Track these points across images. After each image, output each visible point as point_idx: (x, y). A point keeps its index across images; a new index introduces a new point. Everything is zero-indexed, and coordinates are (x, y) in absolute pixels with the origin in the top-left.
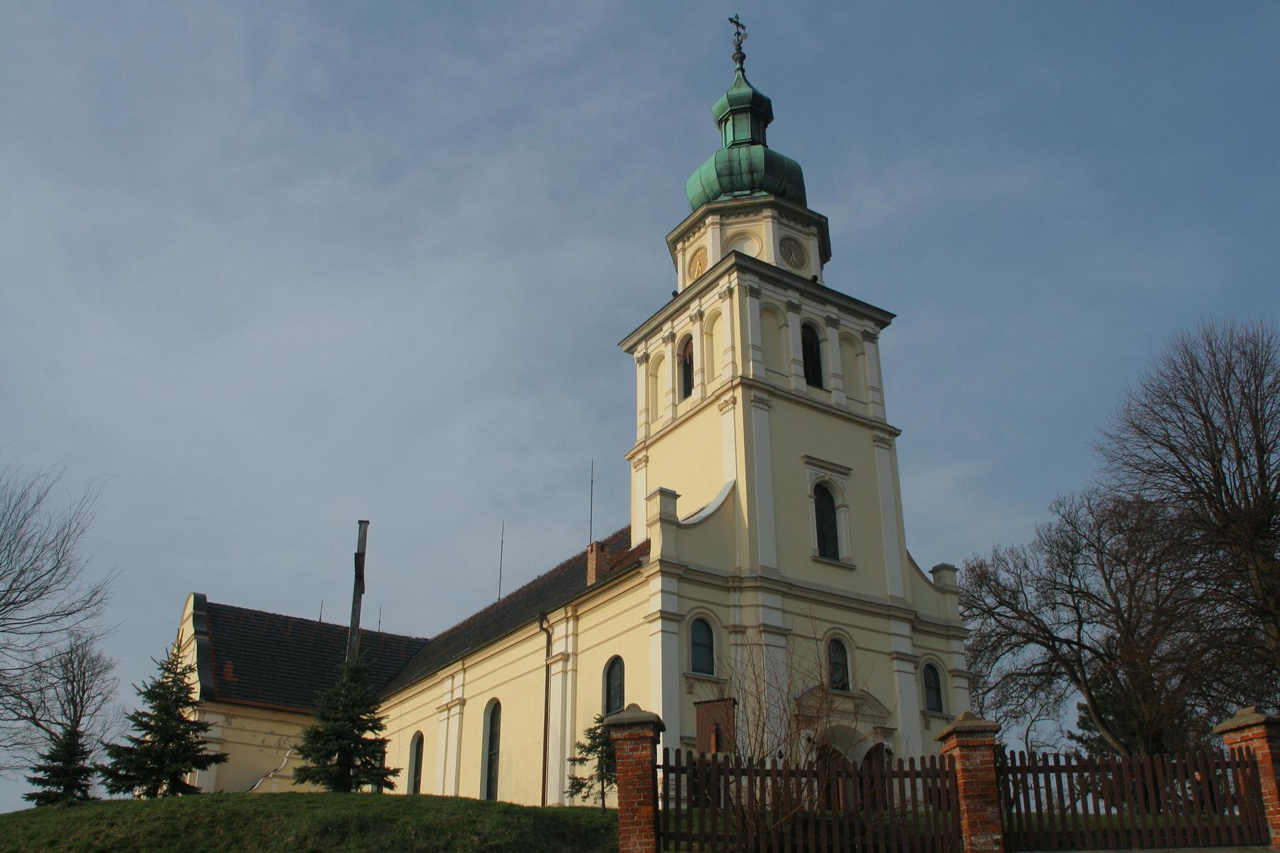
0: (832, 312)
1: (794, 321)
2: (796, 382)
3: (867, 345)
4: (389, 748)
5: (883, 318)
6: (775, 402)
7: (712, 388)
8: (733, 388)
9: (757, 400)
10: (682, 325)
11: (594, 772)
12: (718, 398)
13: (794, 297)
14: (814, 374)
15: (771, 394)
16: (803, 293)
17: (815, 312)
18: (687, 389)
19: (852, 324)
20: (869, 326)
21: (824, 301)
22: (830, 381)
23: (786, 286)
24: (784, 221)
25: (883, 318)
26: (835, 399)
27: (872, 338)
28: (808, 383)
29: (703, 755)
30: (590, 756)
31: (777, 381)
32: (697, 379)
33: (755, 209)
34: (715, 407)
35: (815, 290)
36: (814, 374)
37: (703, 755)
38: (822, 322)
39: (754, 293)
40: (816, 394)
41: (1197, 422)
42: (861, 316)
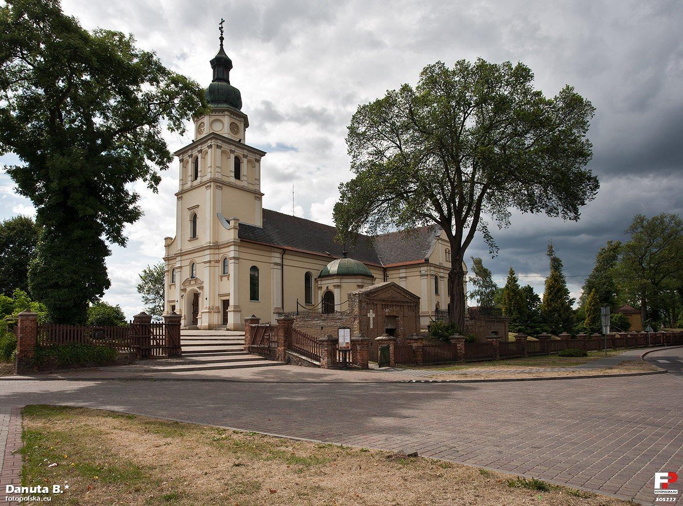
0: (246, 153)
1: (232, 156)
2: (233, 180)
3: (257, 164)
4: (534, 290)
6: (224, 187)
7: (205, 179)
8: (210, 182)
9: (217, 186)
10: (195, 152)
11: (140, 180)
12: (206, 184)
13: (233, 148)
14: (237, 176)
15: (223, 184)
16: (236, 146)
17: (239, 152)
18: (196, 177)
19: (252, 156)
20: (258, 157)
21: (243, 149)
22: (242, 178)
23: (230, 144)
24: (232, 116)
26: (243, 183)
27: (258, 161)
28: (235, 178)
29: (556, 289)
30: (17, 111)
31: (225, 179)
32: (199, 174)
33: (223, 111)
34: (204, 187)
35: (240, 144)
36: (237, 176)
37: (556, 289)
39: (218, 147)
40: (238, 182)
41: (208, 252)
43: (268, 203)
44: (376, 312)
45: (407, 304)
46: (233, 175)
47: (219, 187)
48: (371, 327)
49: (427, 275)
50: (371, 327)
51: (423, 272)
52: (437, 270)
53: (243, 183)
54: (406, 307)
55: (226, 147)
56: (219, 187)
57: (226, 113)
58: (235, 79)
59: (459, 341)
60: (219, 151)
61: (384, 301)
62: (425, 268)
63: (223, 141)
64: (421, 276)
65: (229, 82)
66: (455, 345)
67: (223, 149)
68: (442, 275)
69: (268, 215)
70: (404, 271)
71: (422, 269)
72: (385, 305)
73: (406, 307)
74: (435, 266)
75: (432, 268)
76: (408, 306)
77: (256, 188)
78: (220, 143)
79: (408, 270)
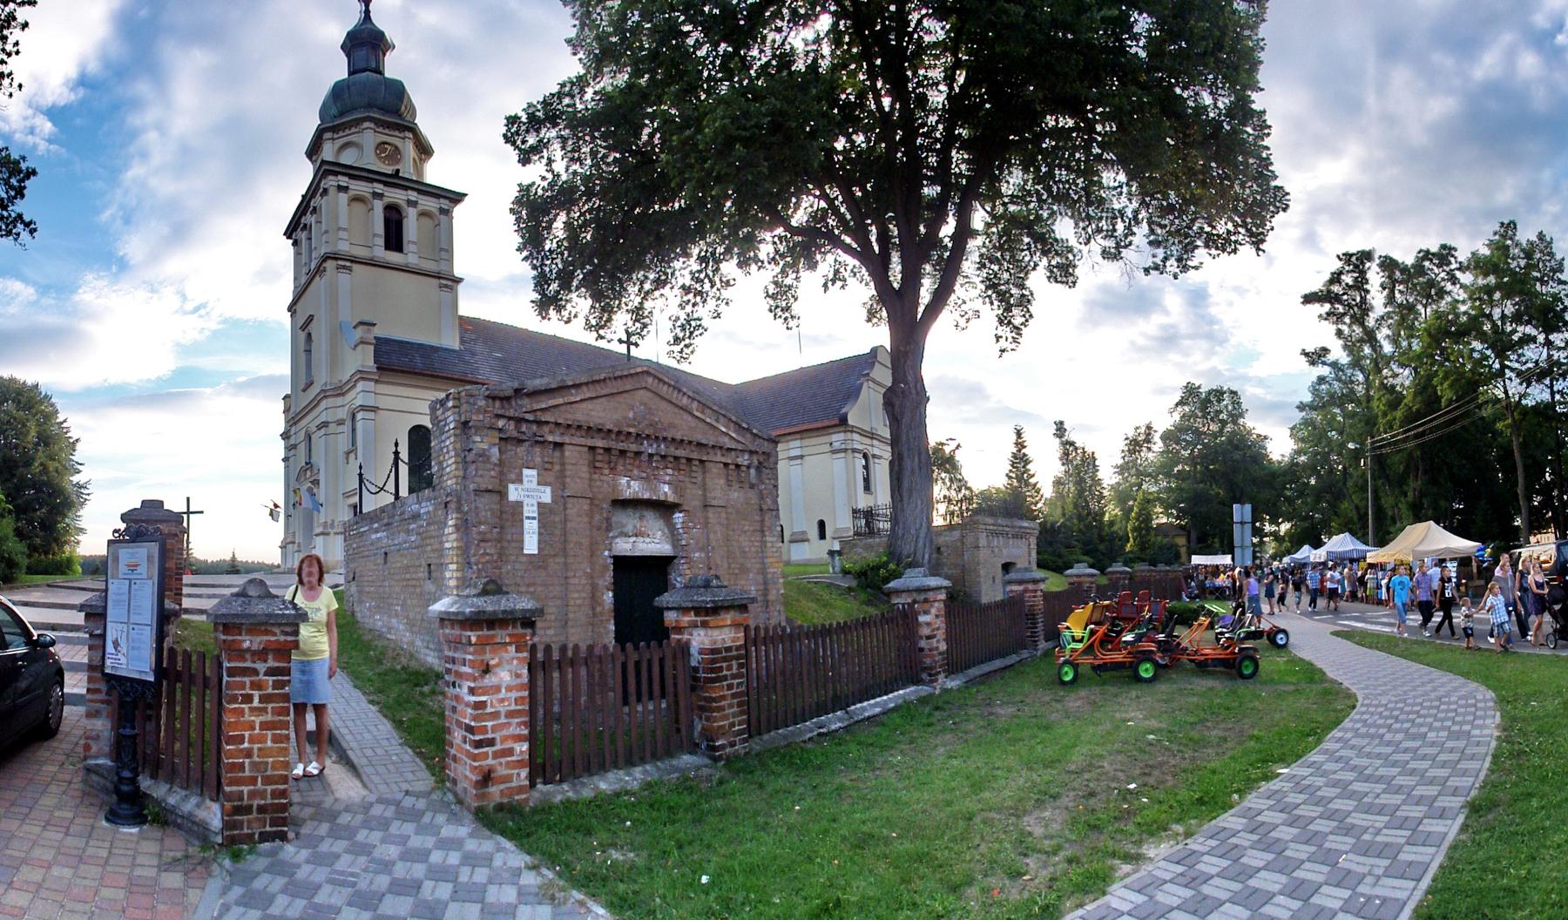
0: (413, 195)
1: (379, 206)
2: (381, 253)
5: (457, 198)
6: (355, 267)
13: (379, 188)
14: (394, 239)
16: (386, 184)
17: (397, 196)
19: (429, 204)
20: (445, 204)
21: (406, 188)
22: (406, 247)
23: (372, 180)
25: (457, 198)
26: (410, 257)
27: (447, 213)
36: (394, 239)
38: (404, 204)
40: (393, 257)
42: (438, 196)
43: (469, 306)
44: (553, 475)
45: (719, 458)
46: (381, 241)
47: (344, 267)
48: (531, 546)
49: (845, 450)
50: (531, 546)
51: (837, 445)
52: (868, 441)
53: (410, 257)
54: (715, 469)
55: (359, 187)
56: (344, 267)
57: (367, 124)
58: (394, 66)
59: (926, 601)
60: (343, 197)
61: (590, 430)
62: (841, 436)
63: (352, 177)
64: (834, 452)
65: (381, 73)
66: (908, 618)
67: (351, 193)
68: (876, 451)
69: (474, 329)
70: (797, 443)
71: (835, 437)
72: (608, 450)
73: (715, 469)
74: (863, 433)
75: (856, 436)
76: (726, 465)
77: (443, 267)
78: (343, 181)
79: (806, 442)
